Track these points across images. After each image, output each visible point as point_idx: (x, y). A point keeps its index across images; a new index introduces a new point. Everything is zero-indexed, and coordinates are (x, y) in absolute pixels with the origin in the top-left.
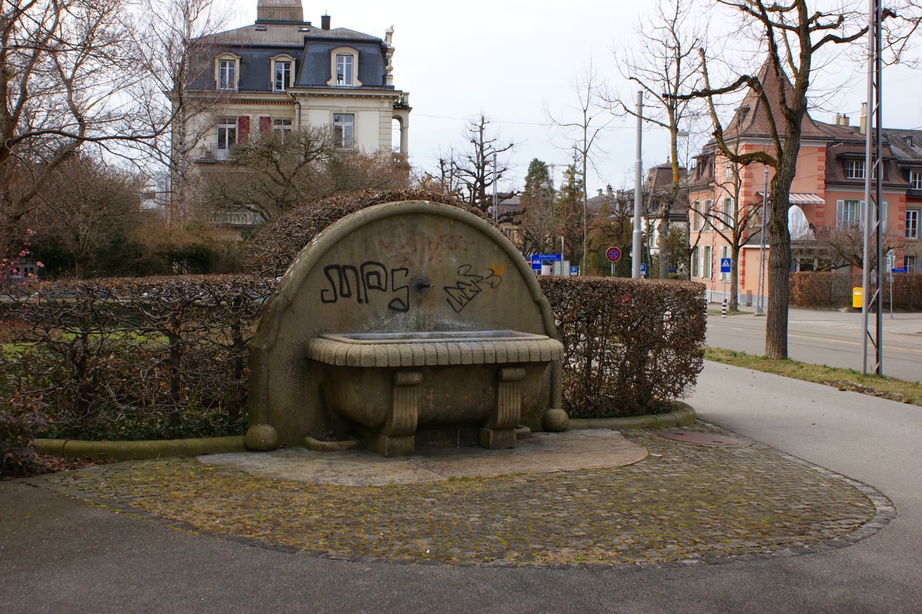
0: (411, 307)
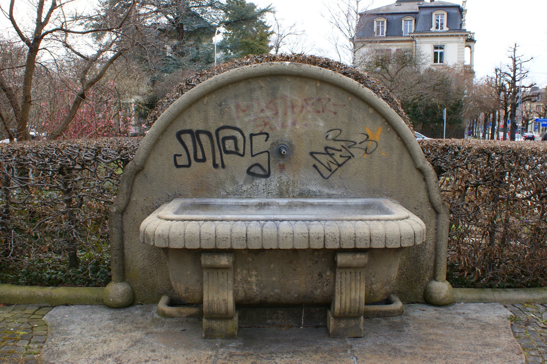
0: (272, 173)
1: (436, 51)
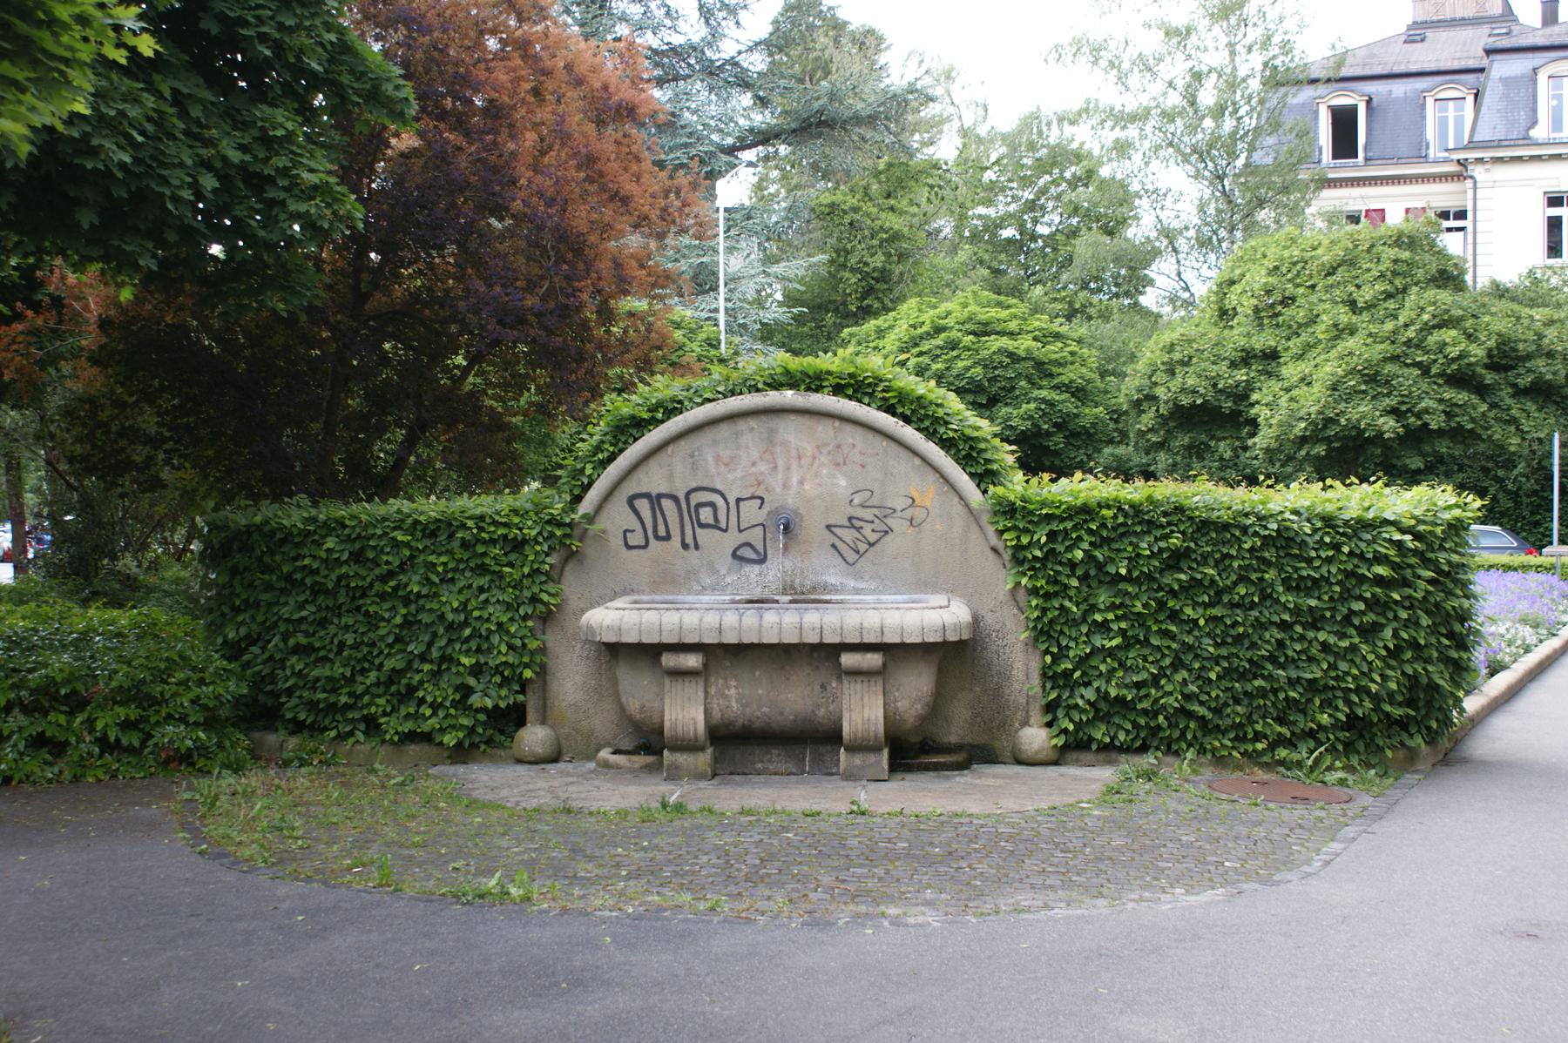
1: (1555, 211)
